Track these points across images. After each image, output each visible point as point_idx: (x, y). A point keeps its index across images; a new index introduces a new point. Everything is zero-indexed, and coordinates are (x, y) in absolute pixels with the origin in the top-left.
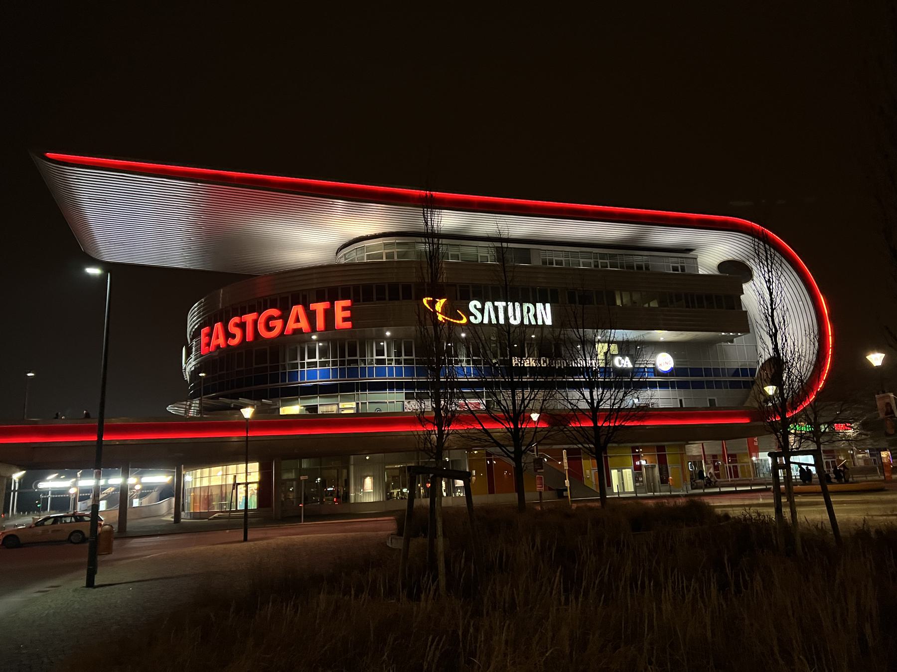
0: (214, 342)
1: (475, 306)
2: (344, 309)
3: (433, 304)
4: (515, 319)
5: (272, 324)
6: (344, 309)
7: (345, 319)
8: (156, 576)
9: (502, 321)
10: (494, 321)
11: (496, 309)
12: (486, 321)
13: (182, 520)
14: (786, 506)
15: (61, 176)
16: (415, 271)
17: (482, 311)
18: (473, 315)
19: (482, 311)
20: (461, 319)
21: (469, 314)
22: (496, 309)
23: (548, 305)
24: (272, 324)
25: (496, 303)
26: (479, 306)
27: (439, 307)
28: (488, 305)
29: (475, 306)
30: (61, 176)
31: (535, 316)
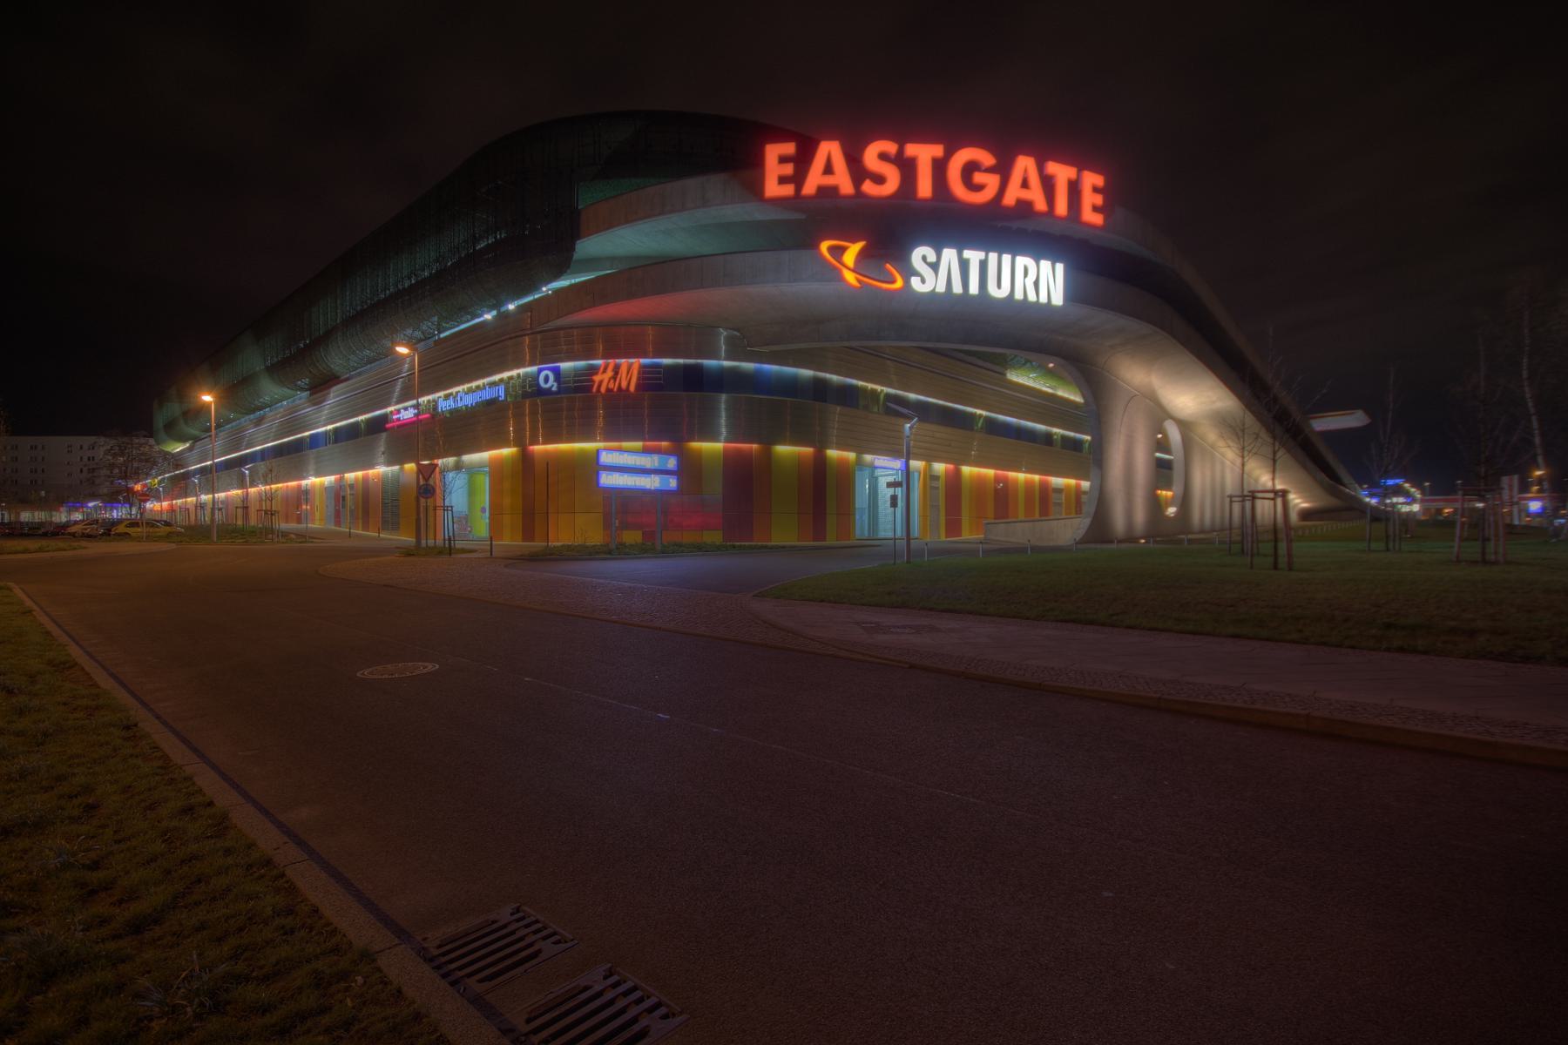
0: (814, 181)
1: (924, 258)
2: (783, 160)
3: (838, 252)
4: (999, 286)
5: (979, 178)
6: (783, 160)
7: (783, 180)
8: (1245, 476)
9: (974, 289)
10: (957, 289)
11: (964, 265)
12: (941, 288)
13: (1091, 217)
14: (18, 514)
15: (512, 943)
16: (39, 998)
17: (935, 267)
18: (917, 274)
19: (935, 267)
20: (894, 282)
21: (909, 272)
22: (964, 265)
23: (1060, 267)
24: (979, 178)
25: (967, 254)
26: (932, 257)
27: (850, 257)
28: (949, 255)
29: (924, 258)
30: (512, 943)
31: (1036, 284)
